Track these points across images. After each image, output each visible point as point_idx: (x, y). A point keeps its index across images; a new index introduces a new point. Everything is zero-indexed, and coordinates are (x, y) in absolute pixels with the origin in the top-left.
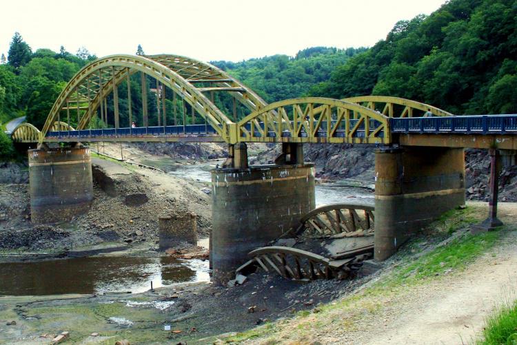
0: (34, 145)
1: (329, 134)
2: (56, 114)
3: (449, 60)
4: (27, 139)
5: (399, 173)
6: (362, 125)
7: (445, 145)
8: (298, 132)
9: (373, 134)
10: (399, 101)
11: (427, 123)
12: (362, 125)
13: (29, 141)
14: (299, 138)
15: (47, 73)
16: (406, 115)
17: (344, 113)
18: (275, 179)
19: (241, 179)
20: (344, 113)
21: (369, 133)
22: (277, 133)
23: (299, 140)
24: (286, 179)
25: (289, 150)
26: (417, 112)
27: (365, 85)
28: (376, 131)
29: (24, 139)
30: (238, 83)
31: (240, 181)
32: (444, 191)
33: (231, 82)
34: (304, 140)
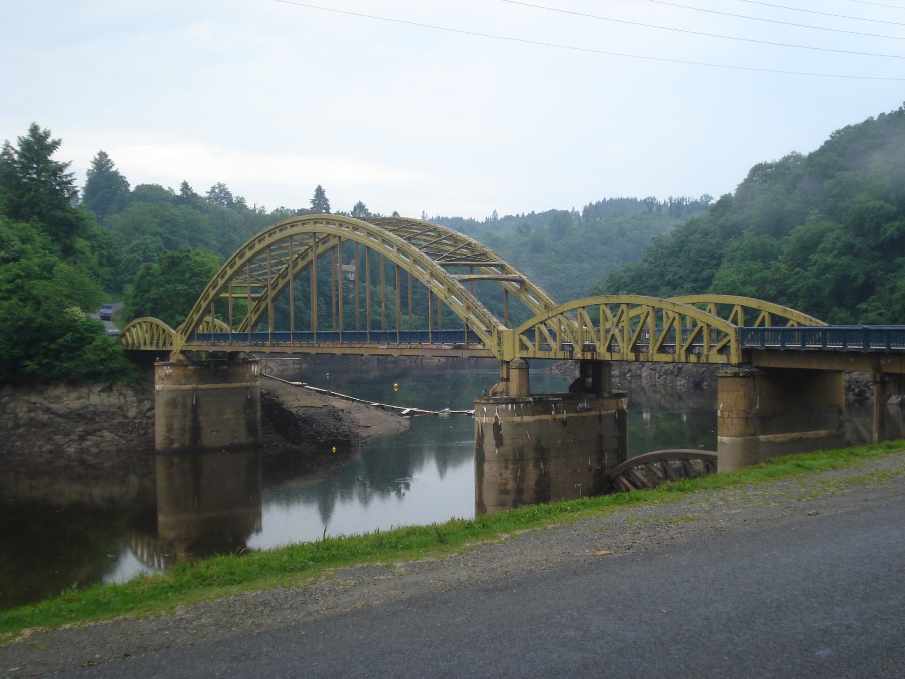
0: (164, 355)
1: (652, 349)
2: (209, 304)
3: (834, 235)
4: (151, 344)
5: (751, 405)
6: (699, 337)
7: (814, 366)
8: (607, 345)
9: (715, 350)
10: (752, 303)
11: (789, 335)
12: (699, 337)
13: (154, 348)
14: (609, 354)
15: (160, 230)
16: (762, 323)
17: (674, 319)
18: (569, 415)
19: (519, 413)
20: (674, 319)
21: (711, 347)
22: (575, 345)
23: (608, 357)
24: (585, 414)
25: (590, 372)
26: (777, 320)
27: (701, 271)
28: (719, 345)
29: (145, 344)
30: (512, 268)
31: (518, 416)
32: (816, 432)
33: (502, 267)
34: (616, 356)
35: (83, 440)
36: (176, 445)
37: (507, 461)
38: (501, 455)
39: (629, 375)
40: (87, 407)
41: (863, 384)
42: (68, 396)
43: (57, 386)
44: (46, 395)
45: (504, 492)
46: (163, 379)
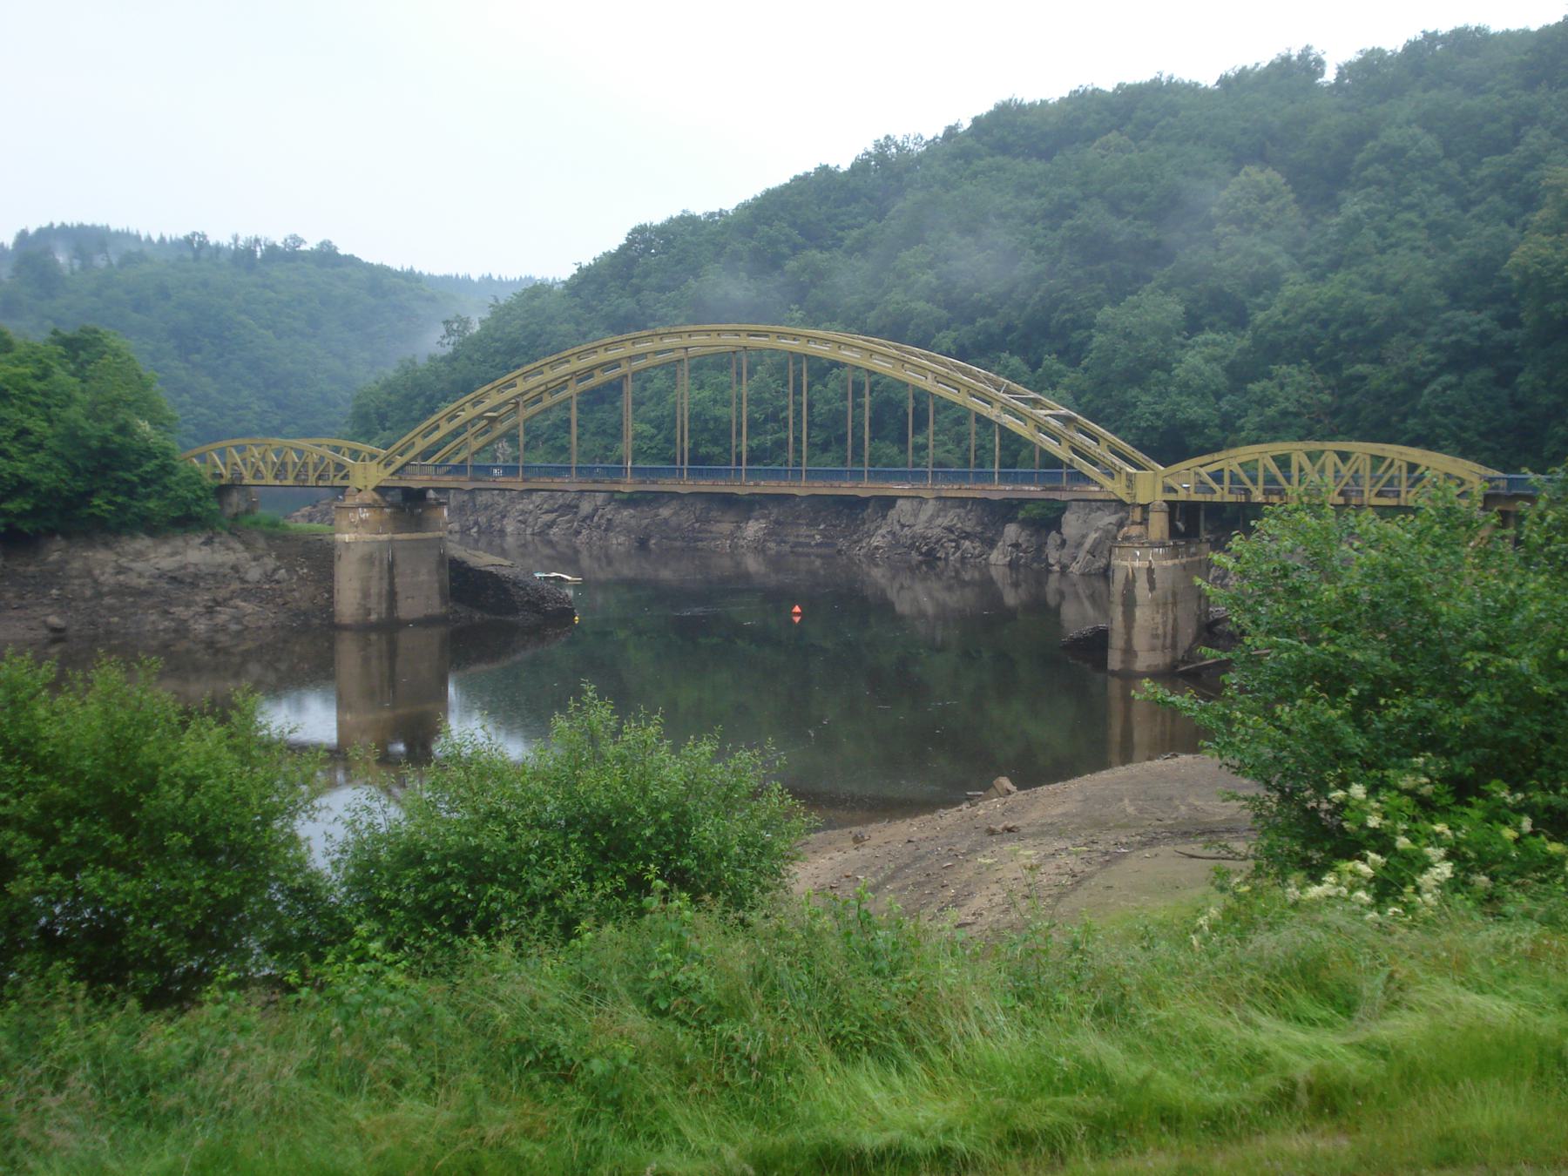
35: (211, 613)
36: (373, 617)
37: (1158, 605)
38: (1153, 599)
39: (475, 530)
40: (184, 567)
41: (933, 540)
42: (156, 551)
43: (133, 536)
44: (119, 550)
45: (1155, 636)
46: (357, 527)
